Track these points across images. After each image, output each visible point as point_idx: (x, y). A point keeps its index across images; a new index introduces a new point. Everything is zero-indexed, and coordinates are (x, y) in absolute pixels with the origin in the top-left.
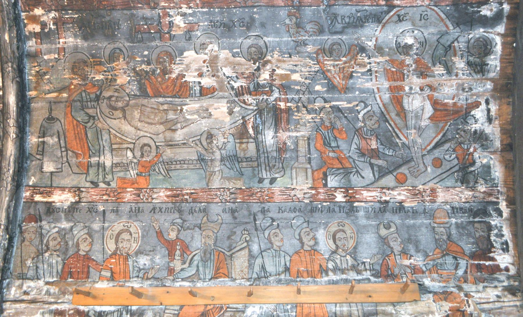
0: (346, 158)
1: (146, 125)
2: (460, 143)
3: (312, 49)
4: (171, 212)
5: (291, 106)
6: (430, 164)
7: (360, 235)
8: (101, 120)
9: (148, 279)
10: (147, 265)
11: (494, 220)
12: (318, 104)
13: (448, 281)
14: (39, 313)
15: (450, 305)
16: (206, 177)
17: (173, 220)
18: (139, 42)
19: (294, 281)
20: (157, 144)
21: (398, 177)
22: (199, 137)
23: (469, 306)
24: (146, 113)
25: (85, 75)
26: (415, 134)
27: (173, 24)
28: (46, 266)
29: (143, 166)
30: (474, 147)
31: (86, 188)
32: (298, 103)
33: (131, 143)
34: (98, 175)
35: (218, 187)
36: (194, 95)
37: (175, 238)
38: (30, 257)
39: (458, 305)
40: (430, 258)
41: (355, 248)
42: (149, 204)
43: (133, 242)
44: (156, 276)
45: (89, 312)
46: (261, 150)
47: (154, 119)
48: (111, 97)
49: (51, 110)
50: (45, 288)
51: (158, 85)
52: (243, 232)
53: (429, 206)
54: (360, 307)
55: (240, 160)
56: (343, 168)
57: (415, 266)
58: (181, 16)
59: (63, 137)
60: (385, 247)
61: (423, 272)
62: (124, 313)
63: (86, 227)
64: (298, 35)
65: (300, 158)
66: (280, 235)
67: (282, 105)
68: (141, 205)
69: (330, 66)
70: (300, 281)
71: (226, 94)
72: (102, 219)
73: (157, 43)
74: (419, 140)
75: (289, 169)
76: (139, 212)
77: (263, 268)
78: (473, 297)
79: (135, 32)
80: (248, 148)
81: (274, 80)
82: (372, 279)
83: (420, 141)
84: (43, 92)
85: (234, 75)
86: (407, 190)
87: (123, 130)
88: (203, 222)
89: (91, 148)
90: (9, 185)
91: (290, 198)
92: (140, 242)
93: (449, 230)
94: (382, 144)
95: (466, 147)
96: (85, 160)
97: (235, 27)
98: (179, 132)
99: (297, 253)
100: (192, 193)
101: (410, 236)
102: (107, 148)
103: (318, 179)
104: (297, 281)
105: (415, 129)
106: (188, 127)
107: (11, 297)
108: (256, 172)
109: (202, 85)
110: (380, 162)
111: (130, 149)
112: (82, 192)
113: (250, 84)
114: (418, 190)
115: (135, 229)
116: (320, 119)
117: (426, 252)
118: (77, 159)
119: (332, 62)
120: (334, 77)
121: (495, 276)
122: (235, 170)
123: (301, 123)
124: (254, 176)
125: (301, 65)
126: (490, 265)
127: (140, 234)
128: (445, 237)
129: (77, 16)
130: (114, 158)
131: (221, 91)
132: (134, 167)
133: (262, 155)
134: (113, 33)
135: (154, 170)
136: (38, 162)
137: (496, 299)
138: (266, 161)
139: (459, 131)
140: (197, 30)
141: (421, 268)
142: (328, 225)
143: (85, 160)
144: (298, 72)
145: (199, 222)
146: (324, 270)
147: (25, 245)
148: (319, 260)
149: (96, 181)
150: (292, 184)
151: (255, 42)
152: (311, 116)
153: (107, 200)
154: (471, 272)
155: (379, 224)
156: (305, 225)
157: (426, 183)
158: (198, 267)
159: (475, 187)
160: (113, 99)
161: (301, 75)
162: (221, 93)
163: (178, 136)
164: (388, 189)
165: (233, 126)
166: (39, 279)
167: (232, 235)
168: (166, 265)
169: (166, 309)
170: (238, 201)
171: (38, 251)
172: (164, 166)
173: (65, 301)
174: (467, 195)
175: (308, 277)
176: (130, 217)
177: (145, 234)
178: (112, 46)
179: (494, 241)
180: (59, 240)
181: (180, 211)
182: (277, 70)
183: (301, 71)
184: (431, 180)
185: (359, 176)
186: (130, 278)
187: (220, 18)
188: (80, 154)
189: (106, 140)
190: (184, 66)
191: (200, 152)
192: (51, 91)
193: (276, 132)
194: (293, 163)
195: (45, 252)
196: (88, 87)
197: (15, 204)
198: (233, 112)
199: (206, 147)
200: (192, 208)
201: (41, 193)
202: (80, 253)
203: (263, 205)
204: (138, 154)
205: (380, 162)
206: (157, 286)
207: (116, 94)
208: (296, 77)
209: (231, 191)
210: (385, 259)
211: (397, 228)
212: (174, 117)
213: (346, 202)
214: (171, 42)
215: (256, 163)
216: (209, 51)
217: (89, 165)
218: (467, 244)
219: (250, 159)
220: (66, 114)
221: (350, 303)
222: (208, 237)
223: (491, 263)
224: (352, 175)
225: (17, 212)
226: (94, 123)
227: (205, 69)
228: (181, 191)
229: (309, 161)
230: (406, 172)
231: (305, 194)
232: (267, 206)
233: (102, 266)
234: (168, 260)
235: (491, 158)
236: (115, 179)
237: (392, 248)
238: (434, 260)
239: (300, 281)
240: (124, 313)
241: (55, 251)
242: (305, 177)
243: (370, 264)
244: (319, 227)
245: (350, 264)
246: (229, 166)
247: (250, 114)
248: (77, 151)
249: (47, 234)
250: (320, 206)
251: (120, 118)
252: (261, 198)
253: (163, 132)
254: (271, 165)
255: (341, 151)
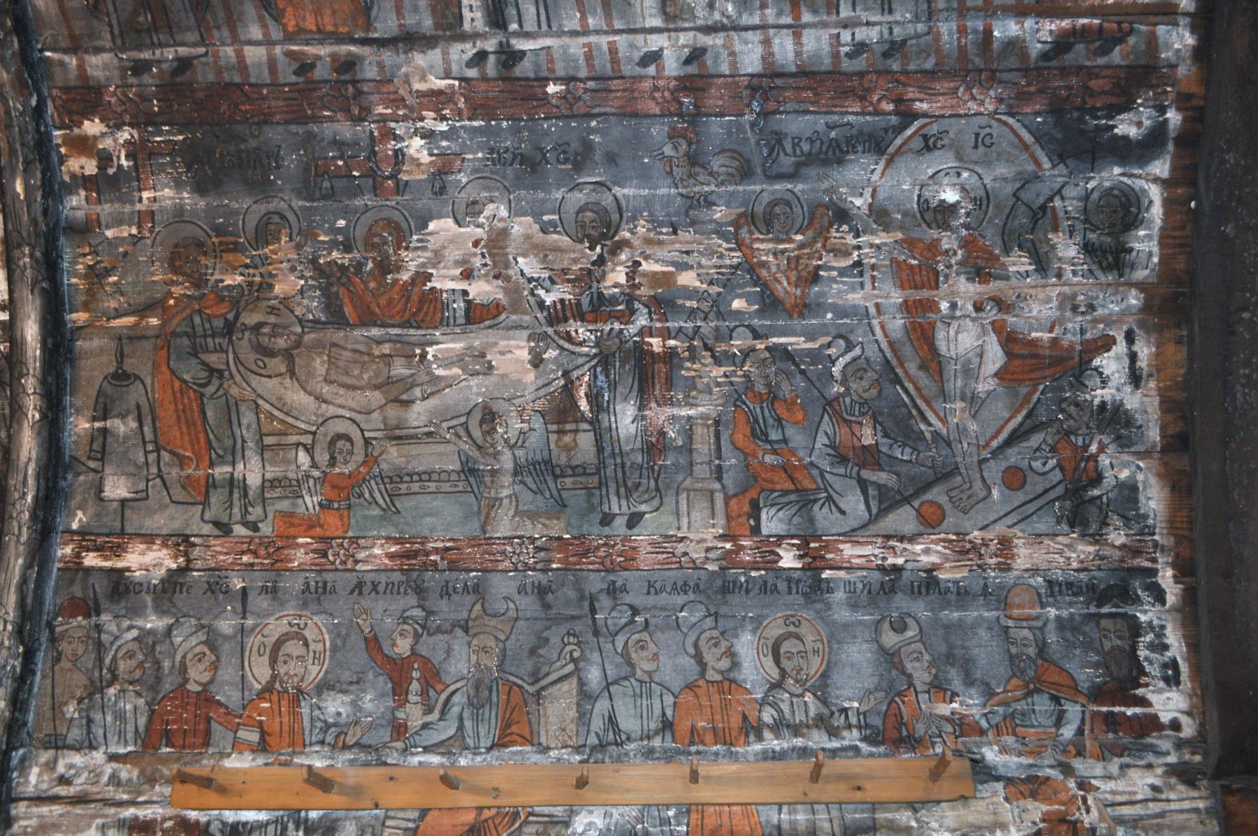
0: (804, 467)
1: (342, 391)
2: (1068, 433)
3: (726, 215)
4: (399, 593)
5: (676, 347)
6: (998, 481)
7: (835, 646)
8: (238, 378)
9: (346, 747)
10: (344, 715)
11: (1145, 612)
12: (738, 344)
13: (1039, 753)
14: (94, 826)
15: (1045, 808)
16: (479, 512)
17: (404, 611)
18: (325, 197)
19: (683, 753)
20: (367, 434)
21: (923, 511)
22: (463, 419)
23: (1088, 811)
24: (341, 364)
25: (201, 274)
26: (963, 410)
27: (404, 155)
28: (109, 719)
29: (333, 487)
30: (1100, 442)
31: (202, 536)
32: (693, 339)
33: (306, 432)
34: (231, 506)
35: (508, 534)
36: (452, 321)
37: (409, 653)
38: (73, 698)
39: (1063, 808)
40: (997, 698)
41: (825, 676)
42: (348, 575)
43: (311, 661)
44: (365, 741)
45: (208, 823)
46: (608, 449)
47: (359, 377)
48: (260, 325)
49: (121, 356)
50: (109, 769)
51: (369, 298)
52: (566, 640)
53: (995, 578)
54: (835, 813)
55: (558, 471)
56: (797, 490)
57: (963, 717)
58: (422, 138)
59: (149, 418)
60: (894, 673)
61: (982, 732)
62: (291, 826)
63: (203, 627)
64: (692, 181)
65: (697, 469)
66: (651, 645)
67: (656, 343)
68: (329, 577)
69: (766, 255)
70: (698, 753)
71: (527, 318)
72: (240, 609)
73: (367, 200)
74: (973, 427)
75: (672, 492)
76: (325, 592)
77: (612, 721)
78: (1098, 788)
79: (316, 175)
80: (576, 444)
81: (638, 287)
82: (864, 747)
83: (975, 428)
84: (104, 314)
85: (545, 274)
86: (944, 540)
87: (289, 401)
88: (473, 616)
89: (215, 444)
90: (25, 530)
91: (674, 559)
92: (327, 662)
93: (1043, 633)
94: (886, 435)
95: (1080, 443)
96: (201, 473)
97: (548, 163)
98: (418, 407)
99: (690, 687)
100: (447, 549)
101: (951, 647)
102: (250, 444)
103: (739, 516)
104: (690, 753)
105: (963, 399)
106: (438, 396)
107: (30, 790)
108: (596, 500)
109: (471, 297)
110: (883, 477)
111: (305, 446)
112: (194, 545)
113: (581, 295)
114: (970, 542)
115: (316, 631)
116: (744, 376)
117: (988, 685)
118: (182, 469)
119: (771, 246)
120: (777, 280)
121: (1149, 740)
122: (547, 495)
123: (700, 386)
124: (591, 508)
125: (699, 252)
126: (1135, 715)
127: (328, 644)
128: (1032, 651)
129: (181, 138)
130: (268, 468)
131: (515, 312)
132: (313, 489)
133: (610, 461)
134: (265, 177)
135: (361, 495)
136: (91, 476)
137: (1149, 794)
138: (620, 474)
139: (1064, 405)
140: (460, 171)
141: (977, 723)
142: (761, 623)
143: (201, 473)
144: (692, 267)
145: (465, 615)
146: (753, 727)
147: (62, 669)
148: (741, 704)
149: (226, 520)
150: (679, 529)
151: (594, 197)
152: (723, 369)
153: (252, 565)
154: (1092, 731)
155: (879, 621)
156: (709, 622)
157: (987, 526)
158: (461, 719)
159: (1102, 535)
160: (266, 330)
161: (698, 275)
162: (514, 317)
163: (415, 416)
164: (901, 539)
165: (542, 392)
166: (95, 749)
167: (540, 647)
168: (388, 716)
169: (387, 817)
170: (554, 566)
171: (92, 682)
172: (382, 487)
173: (155, 799)
174: (1083, 552)
175: (716, 744)
176: (305, 605)
177: (339, 644)
178: (262, 208)
179: (1146, 659)
180: (141, 657)
181: (420, 591)
182: (643, 263)
183: (700, 266)
184: (1000, 518)
185: (833, 508)
186: (304, 746)
187: (512, 142)
188: (188, 458)
189: (249, 427)
190: (428, 254)
191: (466, 454)
192: (121, 312)
193: (642, 407)
194: (680, 478)
195: (109, 686)
196: (208, 304)
197: (38, 573)
198: (542, 360)
199: (480, 441)
200: (447, 582)
201: (98, 549)
202: (189, 687)
203: (612, 577)
204: (323, 457)
205: (883, 477)
206: (367, 764)
207: (272, 319)
208: (687, 279)
209: (538, 543)
210: (893, 701)
211: (921, 630)
212: (407, 372)
213: (802, 569)
214: (399, 198)
215: (596, 479)
216: (488, 218)
217: (211, 484)
218: (1083, 667)
219: (581, 470)
220: (156, 366)
221: (812, 804)
222: (485, 649)
223: (1138, 710)
224: (816, 507)
225: (43, 593)
226: (221, 385)
227: (477, 262)
228: (422, 543)
229: (719, 473)
230: (943, 500)
231: (708, 550)
232: (620, 578)
233: (240, 717)
234: (391, 704)
235: (1139, 467)
236: (271, 516)
237: (910, 676)
238: (1006, 704)
239: (698, 753)
240: (291, 826)
241: (131, 683)
242: (707, 512)
243: (859, 714)
244: (742, 626)
245: (812, 713)
246: (533, 486)
247: (582, 365)
248: (181, 452)
249: (112, 643)
250: (743, 579)
251: (281, 375)
252: (608, 561)
253: (381, 407)
254: (629, 484)
255: (793, 452)
